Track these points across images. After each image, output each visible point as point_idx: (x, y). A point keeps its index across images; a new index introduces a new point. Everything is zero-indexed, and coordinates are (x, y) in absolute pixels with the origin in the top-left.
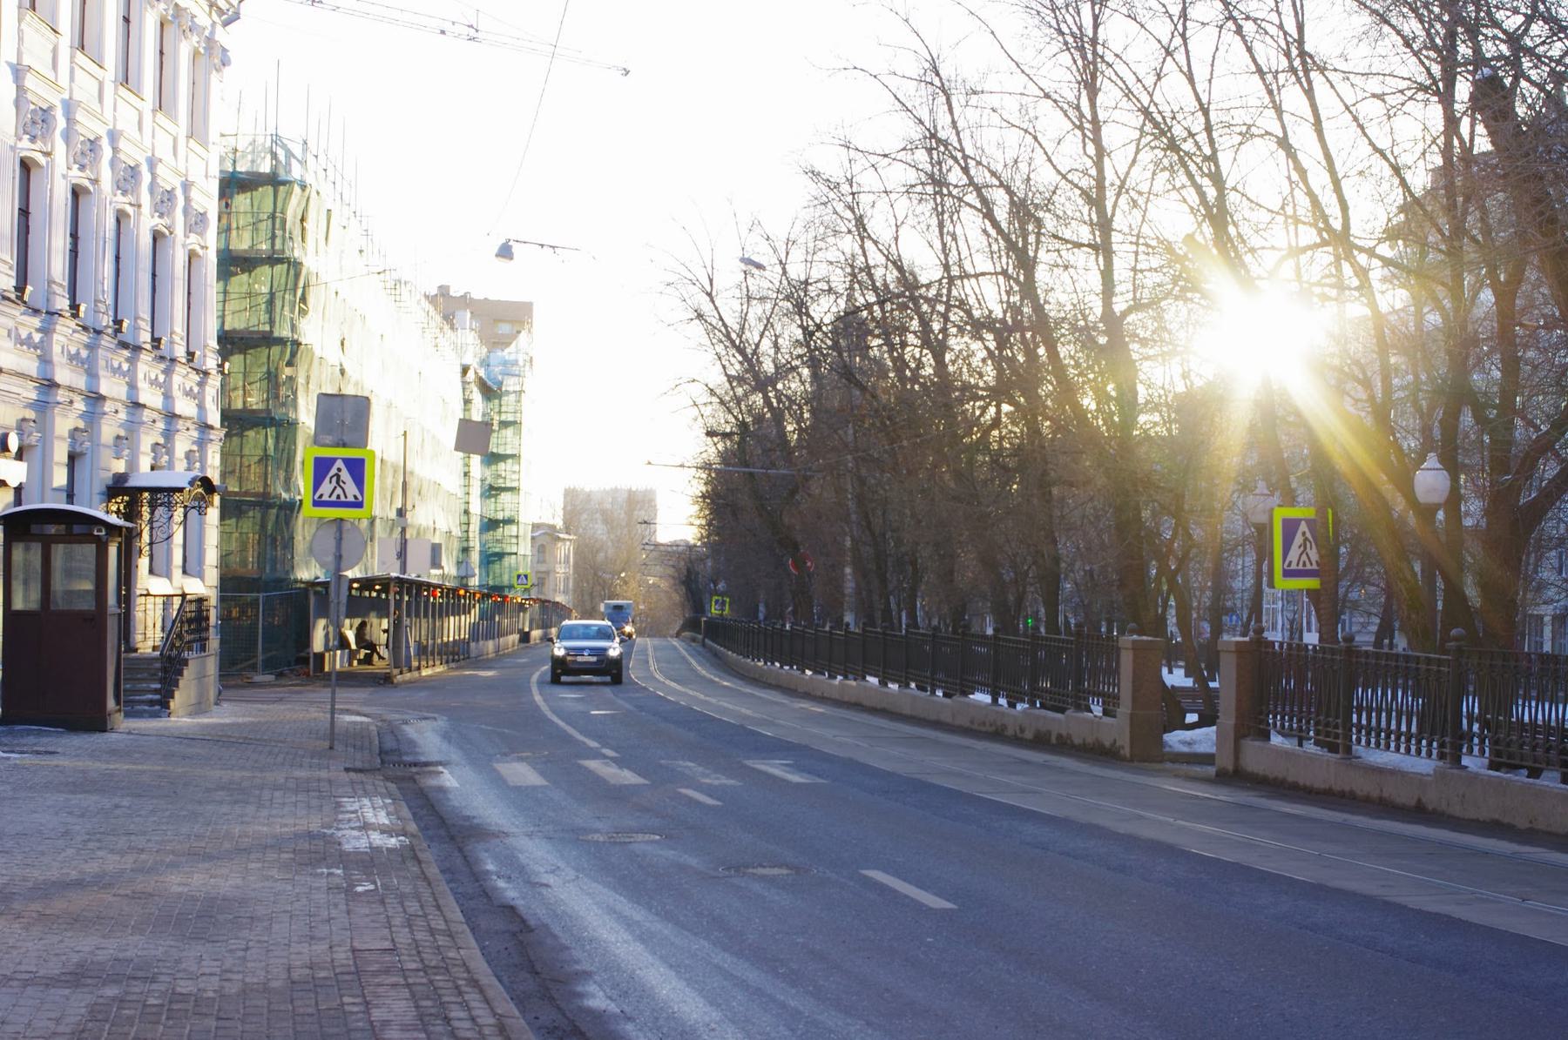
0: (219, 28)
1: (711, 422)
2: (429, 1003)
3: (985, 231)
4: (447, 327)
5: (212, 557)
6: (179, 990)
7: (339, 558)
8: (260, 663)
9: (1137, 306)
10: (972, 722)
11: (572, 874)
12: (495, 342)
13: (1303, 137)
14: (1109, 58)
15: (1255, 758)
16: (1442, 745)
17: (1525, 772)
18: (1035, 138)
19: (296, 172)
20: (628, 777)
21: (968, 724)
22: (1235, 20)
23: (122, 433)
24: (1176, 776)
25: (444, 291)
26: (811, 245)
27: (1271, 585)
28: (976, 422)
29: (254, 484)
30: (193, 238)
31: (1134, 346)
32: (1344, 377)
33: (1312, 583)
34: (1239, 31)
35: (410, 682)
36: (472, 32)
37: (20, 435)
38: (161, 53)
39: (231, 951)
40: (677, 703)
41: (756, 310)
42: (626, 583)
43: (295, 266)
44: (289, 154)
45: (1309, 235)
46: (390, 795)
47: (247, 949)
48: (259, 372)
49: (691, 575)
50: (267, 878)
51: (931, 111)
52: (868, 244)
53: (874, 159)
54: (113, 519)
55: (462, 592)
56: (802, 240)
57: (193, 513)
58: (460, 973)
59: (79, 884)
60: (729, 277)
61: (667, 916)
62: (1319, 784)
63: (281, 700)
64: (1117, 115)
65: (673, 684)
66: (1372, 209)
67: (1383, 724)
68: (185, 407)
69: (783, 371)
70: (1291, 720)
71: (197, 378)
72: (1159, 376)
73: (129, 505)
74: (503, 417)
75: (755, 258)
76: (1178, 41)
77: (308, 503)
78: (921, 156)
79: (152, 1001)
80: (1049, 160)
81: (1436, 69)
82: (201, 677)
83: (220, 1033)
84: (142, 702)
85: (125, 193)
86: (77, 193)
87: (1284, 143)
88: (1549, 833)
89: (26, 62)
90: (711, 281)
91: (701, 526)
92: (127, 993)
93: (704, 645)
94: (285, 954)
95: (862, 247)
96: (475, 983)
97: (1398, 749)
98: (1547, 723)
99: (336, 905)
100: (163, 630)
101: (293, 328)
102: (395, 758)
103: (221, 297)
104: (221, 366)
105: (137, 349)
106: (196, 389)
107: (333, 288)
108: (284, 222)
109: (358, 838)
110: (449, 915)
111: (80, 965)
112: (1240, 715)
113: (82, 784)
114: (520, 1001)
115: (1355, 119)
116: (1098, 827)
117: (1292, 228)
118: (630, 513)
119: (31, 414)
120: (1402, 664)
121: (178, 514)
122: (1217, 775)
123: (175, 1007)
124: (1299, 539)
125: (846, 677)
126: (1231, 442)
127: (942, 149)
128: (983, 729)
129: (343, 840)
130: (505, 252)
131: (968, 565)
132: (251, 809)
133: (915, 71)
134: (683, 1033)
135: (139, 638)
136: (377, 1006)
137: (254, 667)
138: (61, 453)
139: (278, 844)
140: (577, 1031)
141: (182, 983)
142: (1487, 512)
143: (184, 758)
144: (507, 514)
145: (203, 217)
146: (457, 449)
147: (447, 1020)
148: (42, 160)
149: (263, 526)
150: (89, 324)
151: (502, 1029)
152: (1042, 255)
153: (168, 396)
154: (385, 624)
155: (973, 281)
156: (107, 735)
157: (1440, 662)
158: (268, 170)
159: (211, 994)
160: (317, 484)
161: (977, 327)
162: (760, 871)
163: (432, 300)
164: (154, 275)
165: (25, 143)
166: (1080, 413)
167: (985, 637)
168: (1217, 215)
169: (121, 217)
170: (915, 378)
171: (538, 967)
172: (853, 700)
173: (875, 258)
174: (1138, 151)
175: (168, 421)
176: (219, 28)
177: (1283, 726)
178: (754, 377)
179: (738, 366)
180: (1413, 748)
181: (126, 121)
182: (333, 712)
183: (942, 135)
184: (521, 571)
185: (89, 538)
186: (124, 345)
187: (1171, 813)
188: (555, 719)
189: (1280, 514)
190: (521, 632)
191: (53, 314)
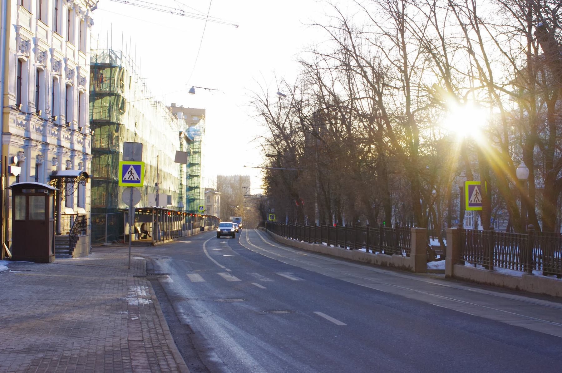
0: (90, 12)
1: (268, 152)
2: (153, 359)
5: (88, 200)
6: (65, 355)
11: (210, 313)
13: (476, 48)
14: (408, 20)
15: (459, 271)
16: (525, 266)
19: (119, 63)
20: (234, 279)
21: (358, 259)
23: (55, 156)
24: (431, 278)
25: (173, 105)
29: (104, 174)
30: (81, 87)
32: (493, 135)
33: (479, 208)
34: (454, 10)
35: (160, 245)
36: (182, 13)
37: (18, 157)
38: (69, 21)
39: (85, 341)
40: (255, 252)
41: (283, 111)
42: (239, 209)
44: (116, 57)
45: (477, 83)
46: (148, 285)
47: (90, 340)
48: (105, 135)
49: (261, 205)
50: (100, 315)
51: (345, 40)
53: (324, 57)
54: (52, 187)
57: (81, 185)
58: (165, 349)
59: (33, 317)
60: (274, 99)
63: (113, 252)
64: (411, 41)
65: (254, 246)
66: (502, 73)
67: (504, 259)
68: (78, 147)
70: (472, 257)
73: (58, 182)
74: (194, 150)
75: (282, 93)
76: (432, 14)
80: (387, 57)
81: (526, 24)
82: (84, 243)
84: (63, 252)
85: (56, 71)
86: (38, 71)
87: (471, 51)
89: (20, 24)
90: (267, 101)
91: (265, 189)
92: (46, 356)
93: (266, 231)
96: (170, 352)
99: (124, 325)
101: (118, 119)
103: (92, 108)
105: (60, 126)
106: (82, 141)
107: (132, 104)
109: (134, 301)
110: (164, 328)
111: (30, 346)
114: (187, 359)
115: (496, 42)
118: (240, 184)
119: (22, 150)
120: (504, 236)
121: (76, 185)
124: (474, 193)
125: (315, 243)
127: (348, 53)
128: (363, 261)
130: (192, 91)
132: (97, 290)
135: (62, 229)
136: (134, 360)
137: (104, 240)
138: (33, 164)
139: (105, 303)
140: (206, 369)
142: (545, 183)
144: (196, 185)
146: (175, 162)
147: (159, 365)
148: (26, 59)
149: (107, 189)
150: (43, 117)
151: (178, 368)
153: (72, 143)
154: (151, 224)
155: (359, 101)
156: (49, 264)
157: (524, 236)
158: (108, 62)
159: (76, 356)
160: (124, 174)
162: (278, 312)
163: (168, 108)
164: (67, 100)
165: (20, 53)
166: (399, 148)
168: (447, 75)
169: (54, 79)
171: (195, 346)
173: (325, 92)
175: (72, 151)
176: (90, 12)
178: (282, 134)
180: (515, 267)
181: (56, 45)
182: (130, 256)
184: (201, 205)
186: (56, 125)
189: (468, 183)
191: (30, 114)
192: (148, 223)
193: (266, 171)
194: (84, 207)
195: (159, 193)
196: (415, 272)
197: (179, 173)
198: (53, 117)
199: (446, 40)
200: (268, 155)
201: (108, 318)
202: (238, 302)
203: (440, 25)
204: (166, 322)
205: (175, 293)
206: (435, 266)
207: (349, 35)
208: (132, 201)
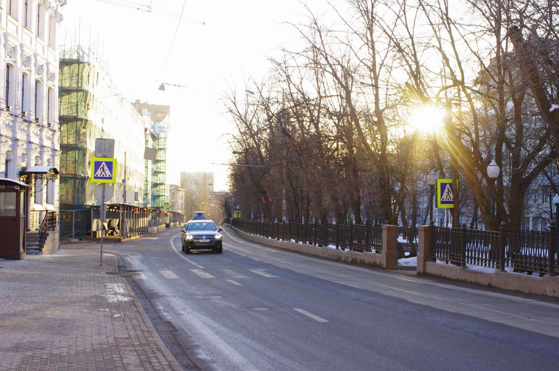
0: (59, 7)
1: (235, 149)
2: (144, 357)
3: (334, 81)
4: (139, 115)
5: (57, 197)
6: (53, 353)
7: (104, 197)
8: (73, 236)
9: (387, 107)
10: (329, 255)
12: (157, 120)
14: (377, 19)
15: (431, 268)
16: (498, 263)
17: (526, 273)
18: (351, 48)
19: (86, 59)
20: (208, 276)
21: (327, 256)
22: (422, 6)
23: (25, 153)
25: (138, 102)
26: (270, 85)
27: (436, 206)
28: (329, 150)
29: (71, 171)
31: (386, 121)
32: (457, 133)
33: (451, 206)
34: (424, 9)
35: (127, 242)
36: (149, 9)
38: (39, 16)
42: (203, 206)
45: (450, 82)
46: (124, 282)
47: (77, 338)
49: (227, 204)
50: (82, 312)
52: (291, 85)
54: (22, 183)
55: (145, 209)
58: (153, 346)
59: (14, 315)
61: (225, 325)
62: (454, 277)
63: (81, 248)
66: (471, 73)
68: (47, 143)
69: (260, 130)
70: (444, 254)
71: (51, 133)
72: (395, 133)
73: (27, 178)
74: (160, 147)
76: (402, 13)
77: (93, 178)
78: (311, 54)
79: (44, 357)
80: (356, 55)
81: (493, 23)
82: (53, 240)
83: (70, 368)
84: (32, 249)
85: (26, 66)
87: (440, 49)
93: (231, 228)
94: (91, 339)
95: (289, 86)
96: (159, 350)
97: (482, 265)
98: (530, 256)
99: (107, 322)
100: (39, 223)
104: (60, 128)
106: (51, 137)
108: (82, 76)
109: (113, 298)
110: (149, 326)
111: (17, 344)
113: (13, 279)
114: (176, 356)
115: (466, 41)
116: (376, 293)
117: (444, 79)
118: (204, 181)
121: (45, 182)
122: (418, 274)
124: (446, 190)
125: (283, 240)
126: (420, 156)
129: (108, 299)
130: (162, 88)
131: (327, 200)
132: (74, 287)
133: (308, 24)
135: (31, 226)
136: (125, 358)
137: (71, 236)
139: (85, 300)
140: (196, 367)
141: (54, 350)
142: (511, 181)
143: (48, 269)
144: (161, 182)
147: (151, 363)
149: (75, 186)
150: (13, 113)
151: (170, 366)
152: (353, 89)
153: (41, 139)
155: (330, 98)
156: (20, 261)
157: (497, 234)
159: (65, 354)
160: (96, 171)
161: (331, 115)
163: (134, 105)
164: (36, 96)
167: (332, 225)
170: (308, 134)
171: (181, 344)
172: (286, 248)
173: (294, 90)
174: (388, 52)
175: (42, 149)
176: (59, 7)
177: (441, 256)
178: (250, 132)
179: (244, 129)
180: (487, 265)
182: (101, 252)
183: (318, 46)
184: (166, 202)
185: (14, 190)
186: (25, 121)
187: (403, 288)
189: (440, 181)
190: (166, 223)
192: (115, 220)
193: (231, 168)
195: (127, 188)
197: (144, 169)
198: (23, 113)
199: (415, 40)
200: (234, 153)
203: (410, 25)
204: (148, 319)
206: (405, 263)
207: (318, 33)
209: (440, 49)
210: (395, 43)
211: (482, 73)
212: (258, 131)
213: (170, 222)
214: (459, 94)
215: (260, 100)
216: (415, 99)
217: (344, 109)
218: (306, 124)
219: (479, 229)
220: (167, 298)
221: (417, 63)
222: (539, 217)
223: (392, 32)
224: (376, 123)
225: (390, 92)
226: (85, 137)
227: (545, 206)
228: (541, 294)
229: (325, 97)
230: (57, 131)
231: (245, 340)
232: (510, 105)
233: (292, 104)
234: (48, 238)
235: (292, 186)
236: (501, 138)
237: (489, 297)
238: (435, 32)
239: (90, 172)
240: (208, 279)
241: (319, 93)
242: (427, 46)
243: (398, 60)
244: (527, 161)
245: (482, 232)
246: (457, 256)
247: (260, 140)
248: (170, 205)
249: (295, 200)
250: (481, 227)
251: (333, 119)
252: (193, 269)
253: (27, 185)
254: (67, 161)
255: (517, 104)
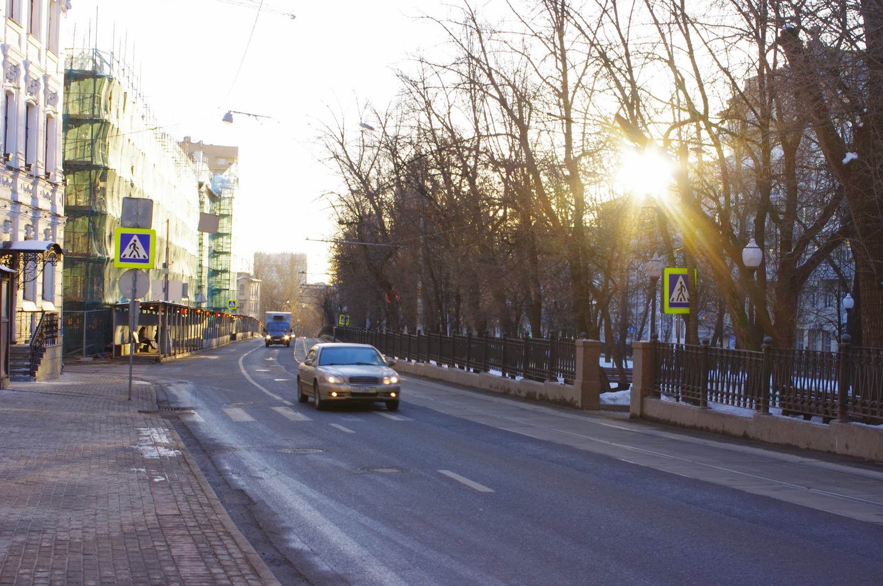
2: (204, 545)
4: (190, 163)
5: (58, 290)
6: (59, 538)
8: (84, 351)
9: (585, 153)
11: (274, 472)
12: (217, 169)
13: (682, 62)
14: (572, 13)
15: (653, 408)
16: (758, 402)
17: (802, 417)
18: (529, 58)
19: (106, 71)
21: (488, 388)
23: (9, 219)
24: (608, 418)
25: (187, 140)
27: (662, 310)
29: (81, 248)
30: (49, 107)
32: (692, 196)
33: (685, 311)
35: (170, 362)
39: (87, 515)
43: (105, 124)
44: (103, 61)
45: (686, 116)
46: (167, 427)
47: (96, 514)
50: (103, 474)
52: (433, 117)
53: (437, 69)
56: (394, 114)
58: (219, 528)
60: (353, 136)
61: (331, 496)
62: (688, 423)
63: (97, 372)
66: (719, 99)
67: (720, 389)
68: (44, 204)
69: (382, 189)
70: (673, 387)
71: (51, 188)
72: (596, 194)
73: (12, 260)
74: (222, 212)
78: (464, 68)
79: (44, 544)
80: (536, 70)
82: (53, 358)
85: (11, 81)
88: (817, 451)
90: (343, 136)
94: (118, 517)
95: (429, 118)
96: (228, 534)
99: (144, 489)
100: (31, 331)
101: (105, 160)
102: (166, 405)
104: (65, 181)
105: (17, 170)
106: (50, 194)
110: (210, 496)
112: (644, 383)
114: (254, 543)
115: (710, 51)
116: (567, 446)
121: (40, 266)
123: (58, 547)
124: (678, 286)
125: (418, 361)
126: (632, 231)
128: (497, 391)
129: (144, 452)
130: (228, 118)
131: (487, 299)
132: (89, 434)
134: (347, 562)
135: (17, 336)
137: (81, 353)
139: (106, 454)
140: (287, 562)
141: (62, 534)
144: (223, 267)
145: (55, 96)
147: (216, 555)
152: (532, 123)
153: (34, 198)
155: (494, 138)
157: (758, 355)
159: (78, 540)
161: (496, 165)
162: (381, 470)
163: (181, 145)
164: (27, 128)
167: (494, 338)
171: (261, 525)
172: (422, 374)
173: (437, 124)
174: (587, 66)
177: (668, 390)
178: (365, 189)
180: (742, 404)
182: (131, 379)
184: (231, 300)
186: (10, 168)
188: (255, 384)
189: (668, 271)
190: (231, 334)
192: (150, 327)
194: (52, 300)
195: (170, 277)
196: (582, 408)
197: (196, 248)
200: (341, 222)
201: (116, 479)
202: (315, 454)
204: (209, 485)
205: (212, 439)
207: (476, 35)
208: (135, 291)
209: (671, 62)
210: (599, 52)
211: (734, 101)
212: (378, 189)
213: (237, 332)
214: (699, 134)
215: (384, 140)
216: (625, 143)
217: (517, 154)
218: (456, 179)
219: (725, 347)
220: (237, 453)
221: (632, 82)
222: (819, 330)
223: (595, 34)
224: (567, 178)
225: (589, 129)
226: (104, 195)
227: (830, 312)
228: (825, 450)
229: (488, 136)
230: (60, 184)
231: (363, 519)
232: (778, 152)
233: (434, 148)
234: (44, 356)
235: (432, 276)
236: (764, 207)
237: (745, 454)
238: (663, 35)
239: (112, 251)
240: (300, 422)
241: (477, 130)
242: (650, 57)
243: (604, 80)
244: (804, 242)
245: (728, 351)
246: (693, 390)
247: (381, 203)
248: (237, 305)
249: (437, 298)
250: (730, 344)
251: (499, 171)
252: (276, 406)
253: (13, 271)
254: (74, 233)
255: (790, 150)
